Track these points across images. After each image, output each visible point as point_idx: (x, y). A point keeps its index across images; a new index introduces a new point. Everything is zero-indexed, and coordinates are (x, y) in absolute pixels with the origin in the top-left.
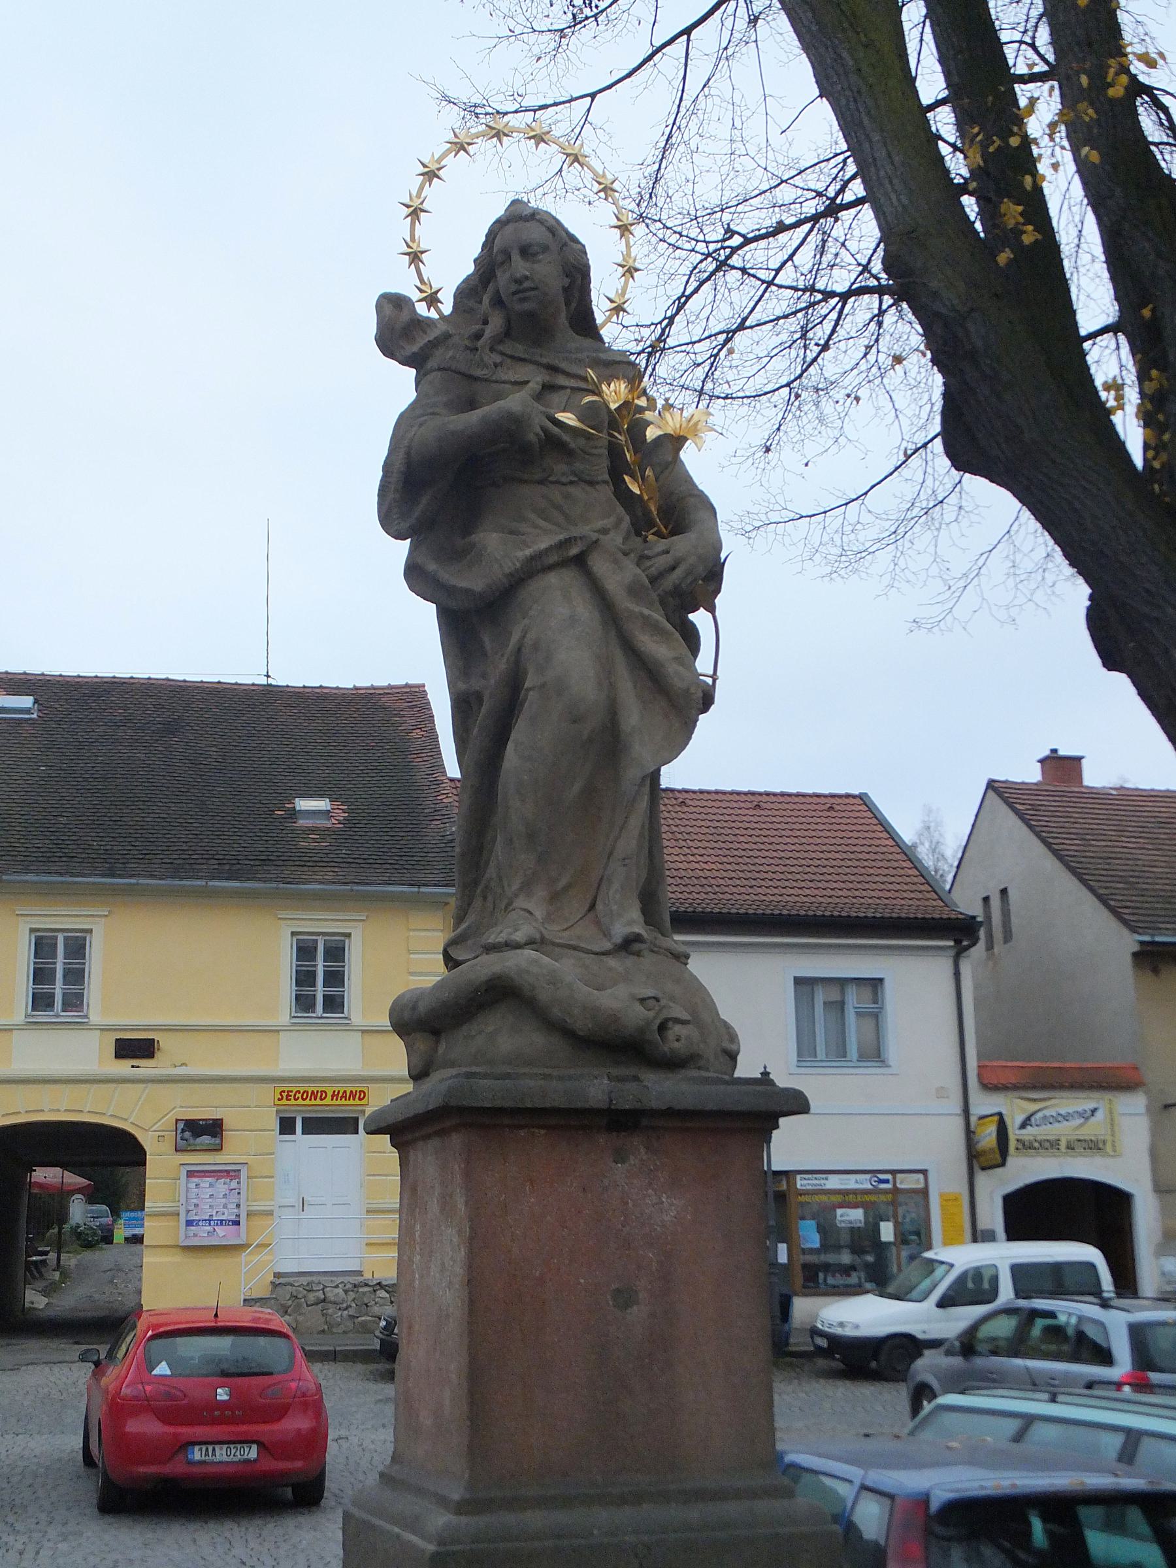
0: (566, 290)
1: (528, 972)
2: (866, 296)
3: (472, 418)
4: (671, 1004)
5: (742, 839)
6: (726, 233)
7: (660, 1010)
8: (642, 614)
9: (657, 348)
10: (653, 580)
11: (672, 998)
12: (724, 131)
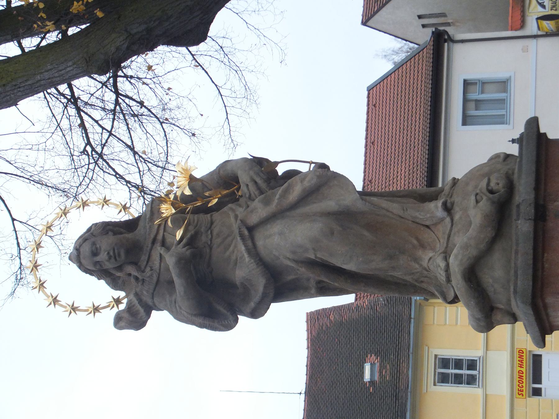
0: (115, 234)
1: (461, 260)
2: (118, 84)
3: (178, 282)
4: (479, 188)
5: (389, 152)
6: (84, 154)
7: (482, 193)
8: (278, 199)
9: (142, 189)
10: (261, 192)
11: (476, 187)
12: (33, 154)
